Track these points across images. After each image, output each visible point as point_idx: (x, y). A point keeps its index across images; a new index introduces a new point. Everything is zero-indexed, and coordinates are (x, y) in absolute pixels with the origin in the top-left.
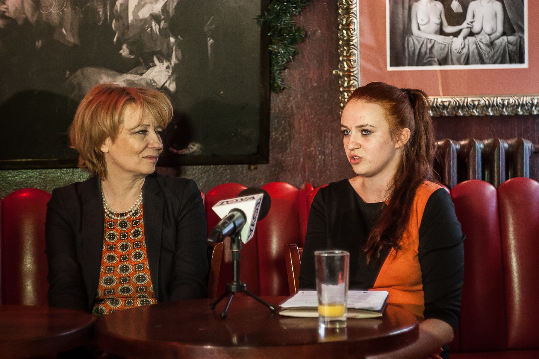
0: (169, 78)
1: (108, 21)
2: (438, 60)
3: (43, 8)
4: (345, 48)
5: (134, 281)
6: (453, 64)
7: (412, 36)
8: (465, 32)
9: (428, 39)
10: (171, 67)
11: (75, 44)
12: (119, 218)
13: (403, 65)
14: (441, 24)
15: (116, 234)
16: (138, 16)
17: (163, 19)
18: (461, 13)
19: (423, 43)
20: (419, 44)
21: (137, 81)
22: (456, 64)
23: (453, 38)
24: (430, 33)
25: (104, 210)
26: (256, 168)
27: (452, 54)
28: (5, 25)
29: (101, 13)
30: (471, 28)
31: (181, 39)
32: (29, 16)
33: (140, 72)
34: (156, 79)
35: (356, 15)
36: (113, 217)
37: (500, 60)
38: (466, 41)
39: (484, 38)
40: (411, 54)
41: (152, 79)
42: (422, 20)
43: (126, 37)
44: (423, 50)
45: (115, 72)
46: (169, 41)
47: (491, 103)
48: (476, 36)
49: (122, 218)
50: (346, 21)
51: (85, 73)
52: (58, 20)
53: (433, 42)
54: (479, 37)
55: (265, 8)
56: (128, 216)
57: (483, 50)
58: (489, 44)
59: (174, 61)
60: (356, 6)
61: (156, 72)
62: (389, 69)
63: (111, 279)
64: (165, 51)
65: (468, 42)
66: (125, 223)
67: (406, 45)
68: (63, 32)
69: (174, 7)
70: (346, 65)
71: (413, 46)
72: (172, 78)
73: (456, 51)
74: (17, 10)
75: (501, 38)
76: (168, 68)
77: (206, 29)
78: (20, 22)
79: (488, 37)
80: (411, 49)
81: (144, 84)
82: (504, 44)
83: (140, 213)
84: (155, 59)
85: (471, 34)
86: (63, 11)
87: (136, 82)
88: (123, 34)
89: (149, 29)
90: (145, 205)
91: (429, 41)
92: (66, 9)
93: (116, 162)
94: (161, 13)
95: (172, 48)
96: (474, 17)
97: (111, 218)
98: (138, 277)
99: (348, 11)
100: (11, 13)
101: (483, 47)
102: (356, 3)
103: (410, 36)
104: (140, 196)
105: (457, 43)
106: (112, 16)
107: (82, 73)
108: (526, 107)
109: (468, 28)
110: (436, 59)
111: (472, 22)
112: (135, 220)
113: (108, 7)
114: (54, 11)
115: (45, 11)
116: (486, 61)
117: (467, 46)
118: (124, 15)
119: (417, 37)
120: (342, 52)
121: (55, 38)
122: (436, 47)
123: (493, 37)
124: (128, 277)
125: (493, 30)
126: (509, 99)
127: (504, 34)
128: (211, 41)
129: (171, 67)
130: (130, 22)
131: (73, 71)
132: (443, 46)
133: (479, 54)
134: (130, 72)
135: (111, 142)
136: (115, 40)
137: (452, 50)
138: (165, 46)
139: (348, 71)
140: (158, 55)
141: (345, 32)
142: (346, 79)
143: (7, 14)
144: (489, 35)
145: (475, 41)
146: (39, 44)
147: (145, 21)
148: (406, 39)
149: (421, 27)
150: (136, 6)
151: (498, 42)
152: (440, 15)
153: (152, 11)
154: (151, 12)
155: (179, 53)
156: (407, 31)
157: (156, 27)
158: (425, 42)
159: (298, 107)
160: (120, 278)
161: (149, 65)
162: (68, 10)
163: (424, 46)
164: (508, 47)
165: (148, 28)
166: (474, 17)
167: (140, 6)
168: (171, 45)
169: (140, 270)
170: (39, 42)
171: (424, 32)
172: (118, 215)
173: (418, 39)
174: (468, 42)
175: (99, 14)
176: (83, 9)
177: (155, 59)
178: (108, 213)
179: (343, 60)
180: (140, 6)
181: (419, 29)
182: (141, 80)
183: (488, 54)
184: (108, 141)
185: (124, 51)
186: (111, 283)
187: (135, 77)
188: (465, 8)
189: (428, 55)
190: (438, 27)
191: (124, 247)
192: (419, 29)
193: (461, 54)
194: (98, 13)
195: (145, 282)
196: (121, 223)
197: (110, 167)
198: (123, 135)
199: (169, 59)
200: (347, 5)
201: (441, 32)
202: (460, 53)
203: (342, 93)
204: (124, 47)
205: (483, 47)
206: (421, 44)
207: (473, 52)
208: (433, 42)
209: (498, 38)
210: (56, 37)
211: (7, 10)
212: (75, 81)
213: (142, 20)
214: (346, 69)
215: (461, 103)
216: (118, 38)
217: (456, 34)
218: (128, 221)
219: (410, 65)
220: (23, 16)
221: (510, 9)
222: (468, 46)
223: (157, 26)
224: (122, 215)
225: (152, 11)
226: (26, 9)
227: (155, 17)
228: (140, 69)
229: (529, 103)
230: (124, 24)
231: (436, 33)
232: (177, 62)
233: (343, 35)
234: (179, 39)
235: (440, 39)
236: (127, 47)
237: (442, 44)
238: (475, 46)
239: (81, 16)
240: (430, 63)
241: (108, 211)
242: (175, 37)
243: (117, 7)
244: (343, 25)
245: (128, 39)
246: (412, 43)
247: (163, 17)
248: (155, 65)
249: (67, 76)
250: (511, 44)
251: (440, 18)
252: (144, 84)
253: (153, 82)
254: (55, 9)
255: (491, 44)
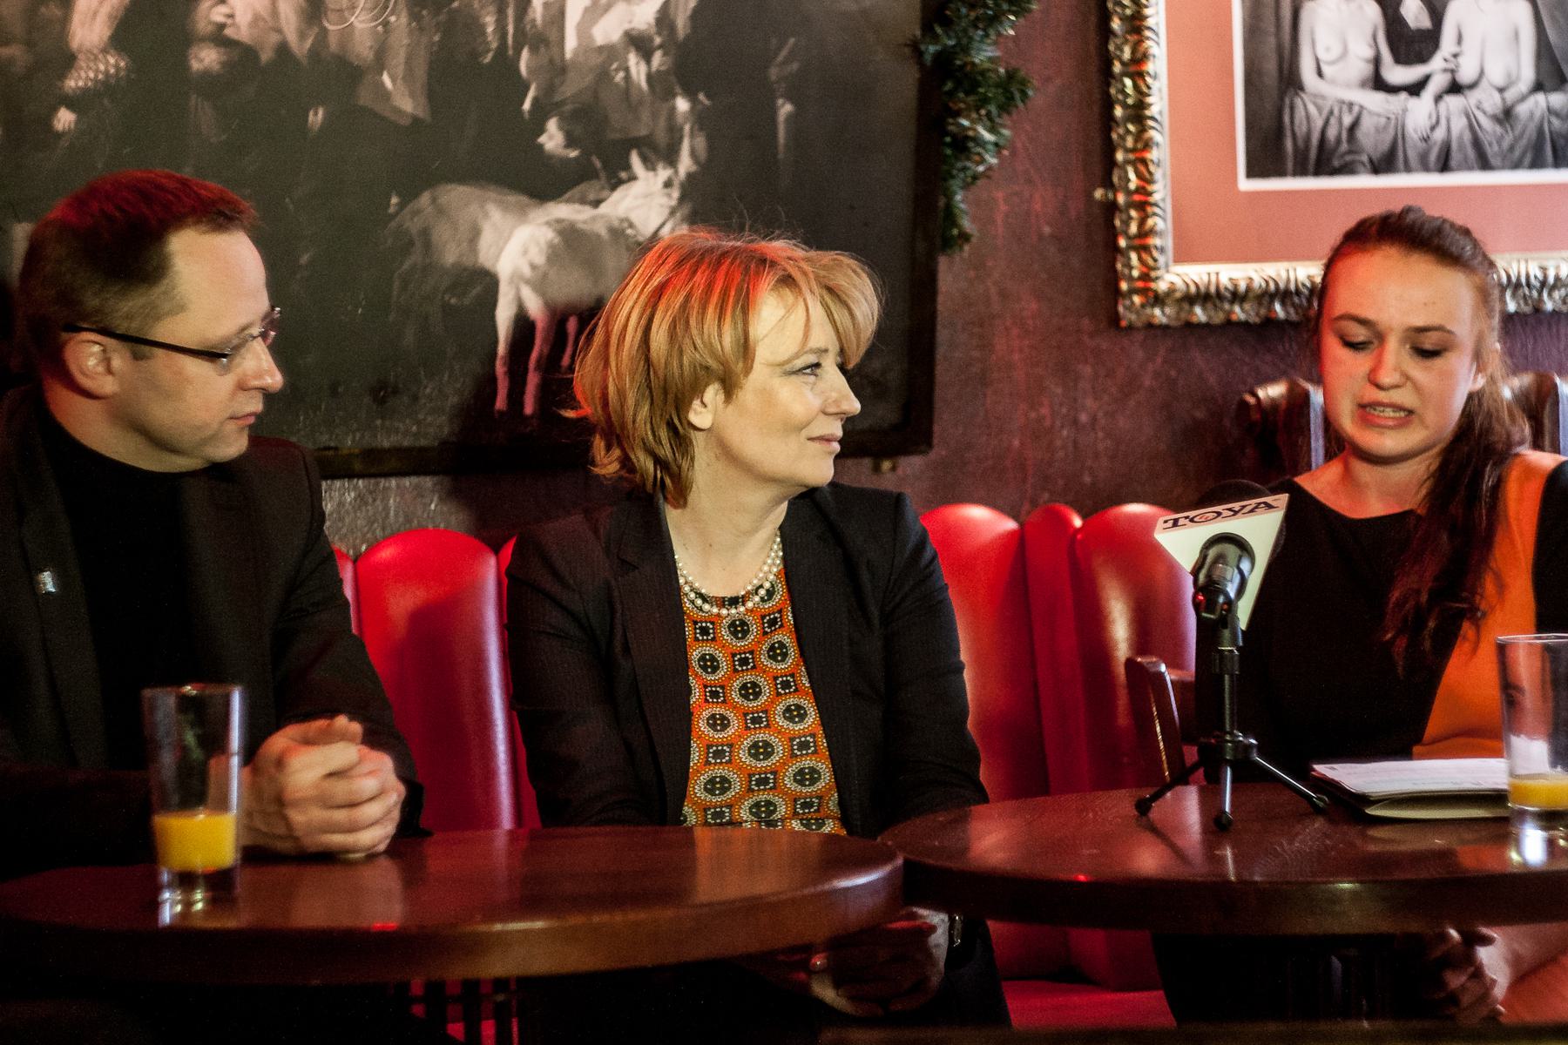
0: (673, 212)
1: (510, 52)
2: (1371, 161)
3: (332, 16)
4: (1131, 127)
5: (789, 783)
6: (1408, 169)
7: (1303, 95)
8: (1438, 82)
9: (1343, 102)
10: (676, 183)
11: (416, 121)
12: (724, 612)
13: (1280, 173)
14: (1377, 61)
15: (719, 655)
16: (591, 37)
17: (660, 47)
18: (1428, 31)
19: (1331, 113)
20: (1320, 114)
21: (585, 222)
22: (1416, 171)
23: (1406, 98)
24: (1348, 86)
25: (679, 588)
26: (894, 469)
27: (1407, 146)
28: (224, 64)
29: (490, 29)
30: (1453, 71)
31: (707, 102)
32: (292, 37)
33: (592, 197)
34: (634, 218)
35: (1157, 34)
36: (706, 607)
37: (1528, 159)
38: (1442, 105)
39: (1487, 100)
40: (1300, 143)
41: (623, 216)
42: (1328, 49)
43: (557, 98)
44: (1332, 133)
45: (524, 199)
46: (673, 109)
47: (1514, 279)
48: (1467, 92)
49: (733, 611)
50: (1133, 52)
51: (443, 200)
52: (371, 47)
53: (1356, 109)
54: (1473, 97)
55: (936, 13)
56: (750, 605)
57: (1487, 132)
58: (1501, 116)
59: (685, 164)
60: (1157, 13)
61: (636, 198)
62: (1246, 185)
63: (724, 780)
64: (661, 137)
65: (1448, 110)
66: (743, 623)
67: (1287, 119)
68: (383, 84)
69: (689, 13)
70: (1132, 175)
71: (1305, 122)
72: (678, 214)
73: (1415, 137)
74: (256, 19)
75: (1532, 100)
76: (668, 184)
77: (773, 73)
78: (266, 56)
79: (1497, 96)
80: (1301, 129)
81: (603, 232)
82: (1538, 114)
83: (781, 594)
84: (635, 160)
85: (1455, 88)
86: (386, 24)
87: (581, 226)
88: (549, 90)
89: (621, 74)
90: (790, 570)
91: (1345, 108)
92: (393, 19)
93: (728, 454)
94: (653, 30)
95: (681, 129)
96: (1460, 40)
97: (701, 609)
98: (801, 772)
99: (1136, 23)
100: (242, 30)
101: (1486, 123)
102: (1157, 4)
103: (1297, 94)
104: (776, 547)
105: (1418, 113)
106: (522, 38)
107: (434, 200)
108: (1296, 300)
109: (1445, 70)
110: (1365, 158)
111: (1455, 56)
112: (769, 615)
113: (510, 12)
114: (361, 23)
115: (337, 24)
116: (1493, 161)
117: (1443, 122)
118: (553, 36)
119: (1315, 96)
120: (1122, 138)
121: (361, 102)
122: (1367, 124)
123: (1510, 95)
124: (771, 773)
125: (1509, 76)
126: (1558, 268)
127: (1538, 87)
128: (785, 109)
129: (676, 183)
130: (568, 55)
131: (409, 196)
132: (1383, 121)
133: (1477, 143)
134: (567, 196)
135: (721, 397)
136: (527, 106)
137: (1406, 131)
138: (662, 123)
139: (1141, 190)
140: (645, 150)
141: (1128, 82)
142: (1133, 213)
143: (228, 32)
144: (1501, 90)
145: (1466, 109)
146: (317, 117)
147: (610, 53)
148: (1287, 101)
149: (1325, 69)
150: (587, 10)
151: (1522, 110)
152: (1375, 38)
153: (630, 22)
154: (627, 26)
155: (701, 142)
156: (1290, 80)
157: (638, 70)
158: (1336, 112)
159: (1004, 295)
160: (750, 776)
161: (617, 176)
162: (400, 20)
163: (1333, 121)
164: (1549, 122)
165: (617, 70)
166: (1460, 40)
167: (595, 11)
168: (680, 119)
169: (804, 752)
170: (316, 114)
171: (1333, 82)
172: (722, 602)
173: (1320, 101)
174: (1448, 110)
175: (484, 33)
176: (442, 18)
177: (635, 160)
178: (692, 595)
179: (1127, 162)
180: (595, 11)
181: (1320, 74)
182: (594, 219)
183: (1497, 142)
184: (712, 393)
185: (551, 138)
186: (724, 790)
187: (579, 212)
188: (1437, 15)
189: (1344, 146)
190: (1366, 70)
191: (749, 691)
192: (1320, 74)
193: (1429, 142)
194: (481, 29)
195: (820, 785)
196: (733, 624)
197: (704, 469)
198: (759, 376)
199: (671, 159)
200: (1134, 7)
201: (1378, 83)
202: (1426, 139)
203: (1124, 253)
204: (552, 125)
205: (1486, 123)
206: (1325, 112)
207: (1460, 138)
208: (1356, 109)
209: (1523, 98)
210: (365, 98)
211: (229, 21)
212: (414, 226)
213: (601, 49)
214: (1132, 186)
215: (1282, 286)
216: (536, 101)
217: (1415, 89)
218: (749, 619)
219: (1301, 170)
220: (274, 38)
221: (1553, 18)
222: (1448, 121)
223: (643, 68)
224: (734, 601)
225: (630, 22)
226: (283, 16)
227: (638, 42)
228: (591, 189)
229: (1304, 285)
230: (551, 61)
231: (1363, 84)
232: (694, 168)
233: (1123, 91)
234: (702, 103)
235: (1375, 102)
236: (561, 128)
237: (1379, 115)
238: (1464, 121)
239: (436, 38)
240: (1347, 169)
241: (691, 590)
242: (690, 94)
243: (534, 12)
244: (1123, 63)
245: (563, 103)
246: (1303, 113)
247: (658, 40)
248: (633, 178)
249: (392, 210)
250: (1557, 114)
251: (1372, 42)
252: (603, 232)
253: (626, 225)
254: (365, 16)
255: (1506, 116)
